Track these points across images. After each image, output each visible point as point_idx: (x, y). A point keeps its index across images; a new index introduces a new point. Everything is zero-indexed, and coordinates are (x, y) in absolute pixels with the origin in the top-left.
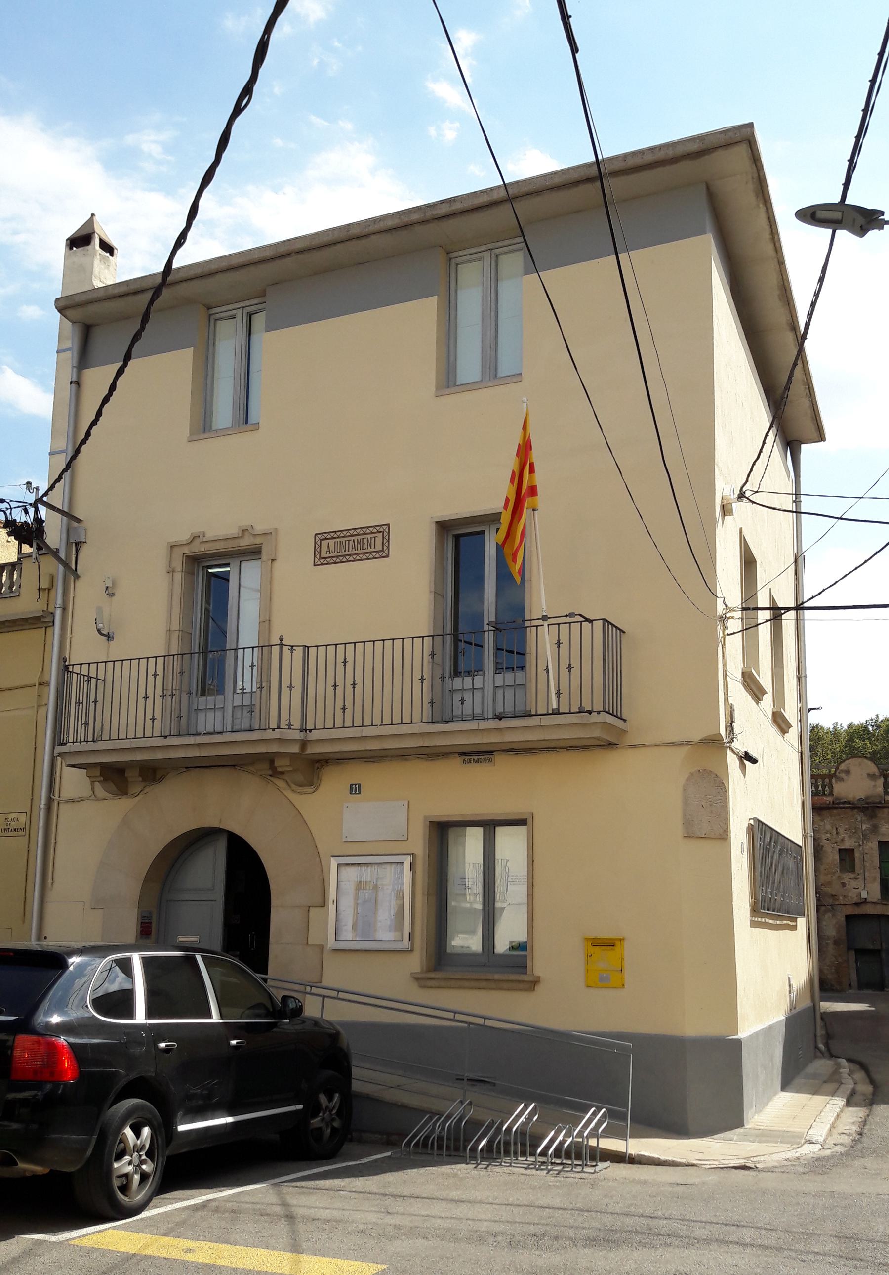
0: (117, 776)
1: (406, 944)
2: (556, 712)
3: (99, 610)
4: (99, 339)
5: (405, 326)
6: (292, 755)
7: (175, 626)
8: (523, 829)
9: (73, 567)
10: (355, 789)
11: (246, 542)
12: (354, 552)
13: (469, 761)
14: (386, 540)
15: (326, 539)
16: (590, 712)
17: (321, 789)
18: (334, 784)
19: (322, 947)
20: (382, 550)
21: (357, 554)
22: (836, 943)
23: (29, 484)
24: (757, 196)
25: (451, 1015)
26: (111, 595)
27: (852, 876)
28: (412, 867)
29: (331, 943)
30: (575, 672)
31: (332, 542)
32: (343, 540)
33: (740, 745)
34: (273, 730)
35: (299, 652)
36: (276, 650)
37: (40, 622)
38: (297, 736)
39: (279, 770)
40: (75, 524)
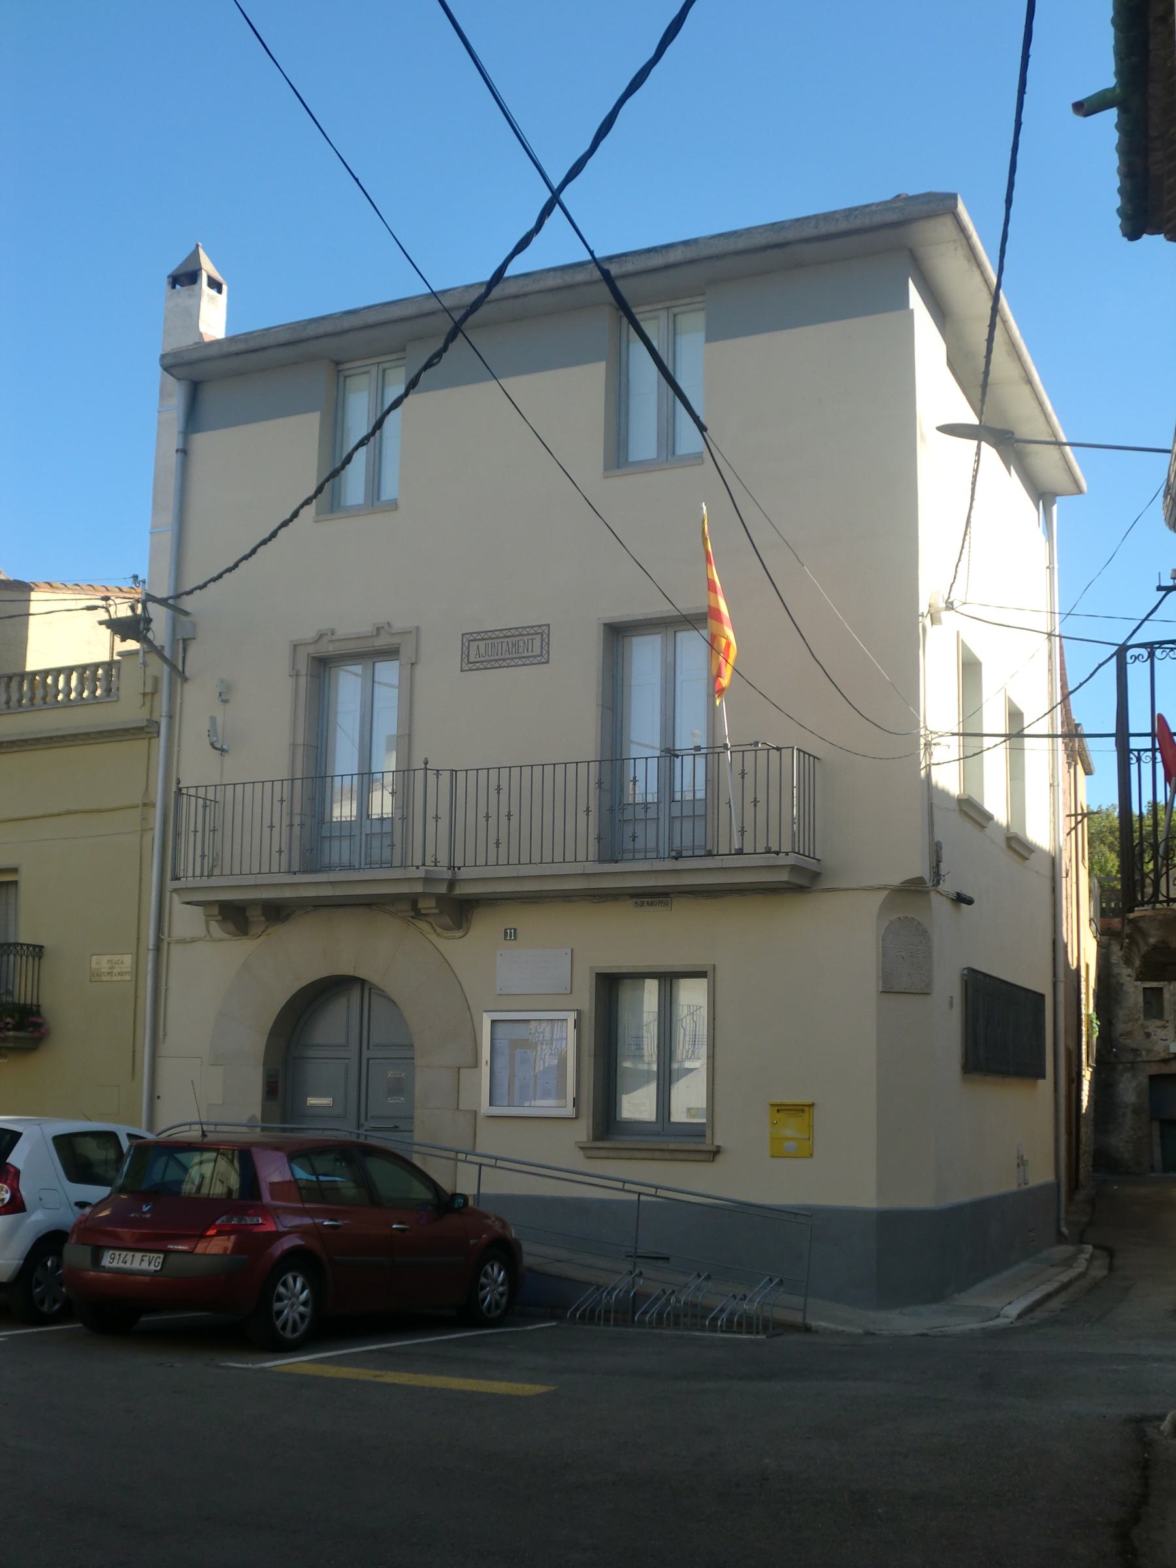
0: (236, 916)
1: (569, 1111)
2: (740, 852)
3: (213, 720)
4: (210, 397)
5: (565, 396)
6: (439, 898)
7: (300, 740)
8: (703, 983)
9: (180, 668)
10: (511, 934)
11: (382, 642)
12: (508, 656)
13: (642, 904)
14: (546, 644)
15: (475, 640)
16: (777, 853)
17: (471, 933)
18: (485, 930)
19: (475, 1113)
20: (541, 655)
21: (512, 659)
22: (1136, 1111)
23: (135, 577)
24: (969, 261)
25: (620, 1185)
26: (225, 701)
27: (1159, 1023)
28: (577, 1024)
29: (485, 1108)
30: (762, 806)
31: (482, 644)
32: (496, 641)
33: (949, 886)
34: (418, 867)
35: (446, 776)
36: (420, 775)
37: (145, 731)
38: (448, 875)
39: (423, 912)
40: (183, 618)
